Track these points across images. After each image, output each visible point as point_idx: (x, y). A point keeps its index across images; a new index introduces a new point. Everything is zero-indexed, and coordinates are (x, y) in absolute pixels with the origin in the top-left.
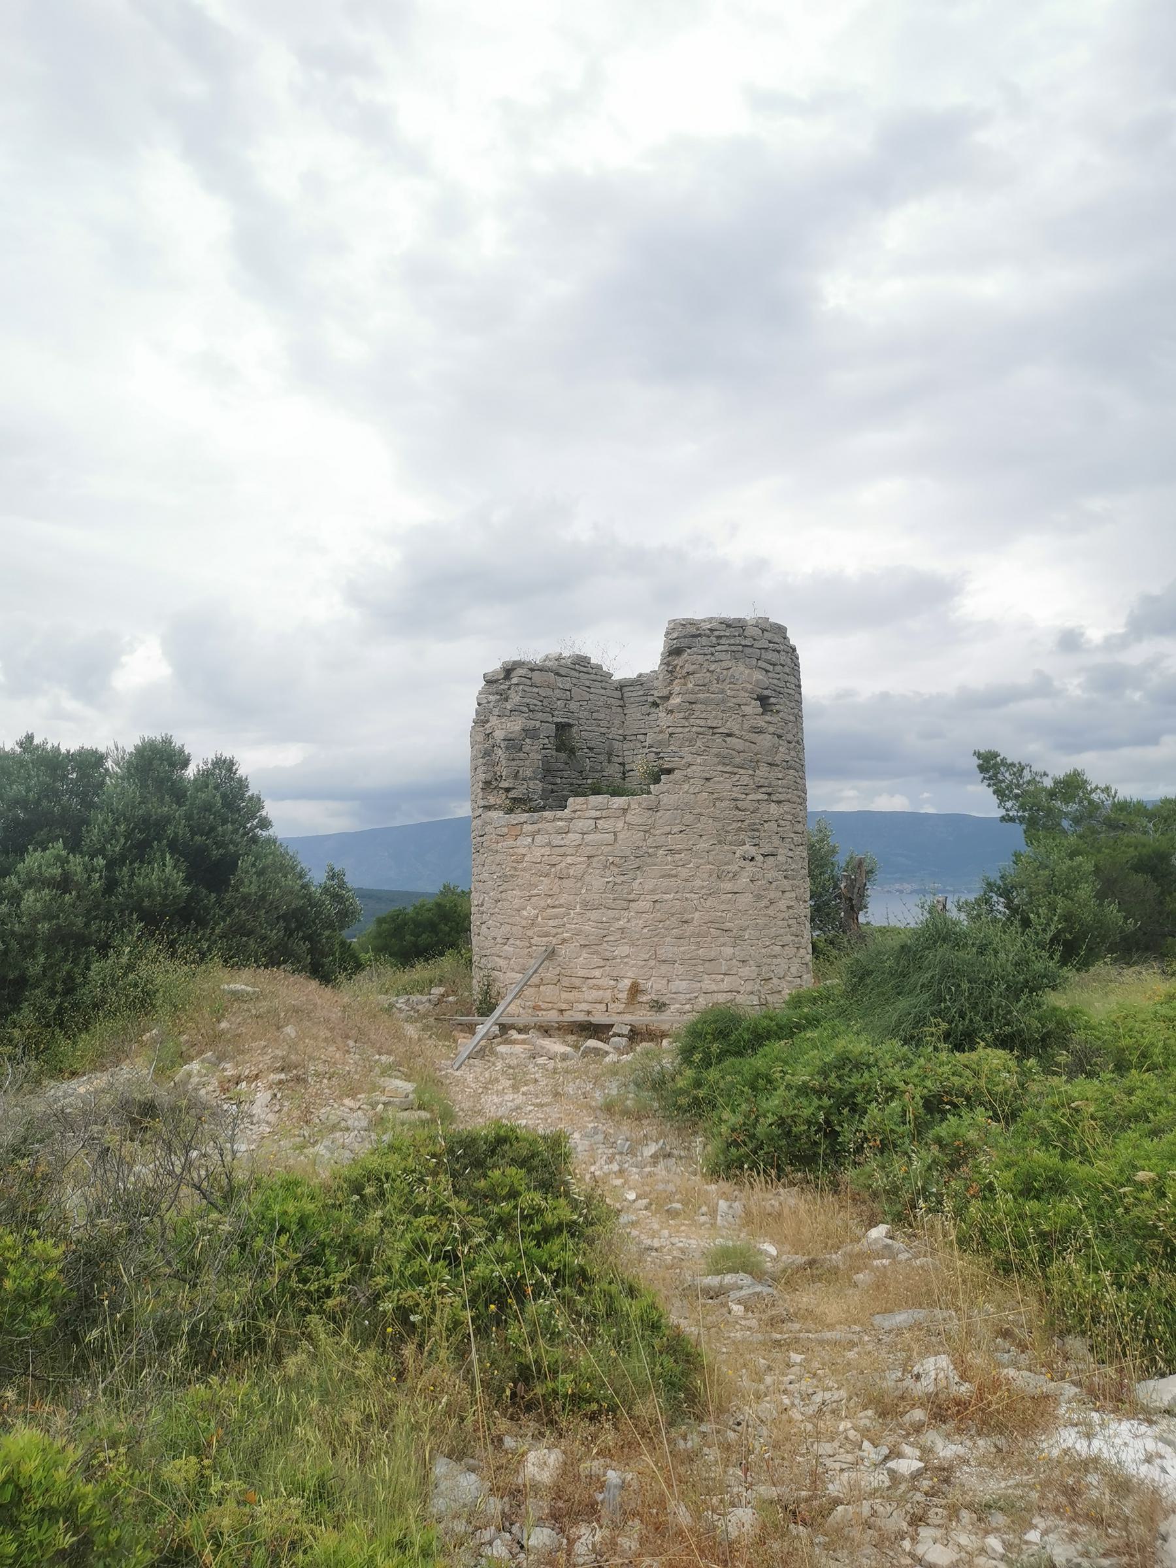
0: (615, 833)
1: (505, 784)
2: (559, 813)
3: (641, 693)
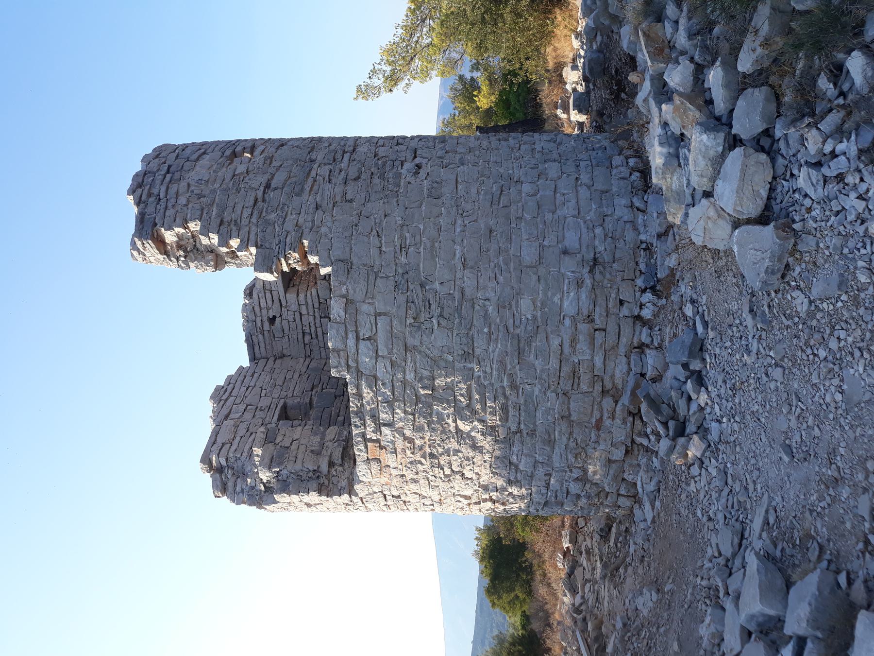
0: (377, 315)
1: (324, 468)
2: (351, 390)
3: (260, 336)
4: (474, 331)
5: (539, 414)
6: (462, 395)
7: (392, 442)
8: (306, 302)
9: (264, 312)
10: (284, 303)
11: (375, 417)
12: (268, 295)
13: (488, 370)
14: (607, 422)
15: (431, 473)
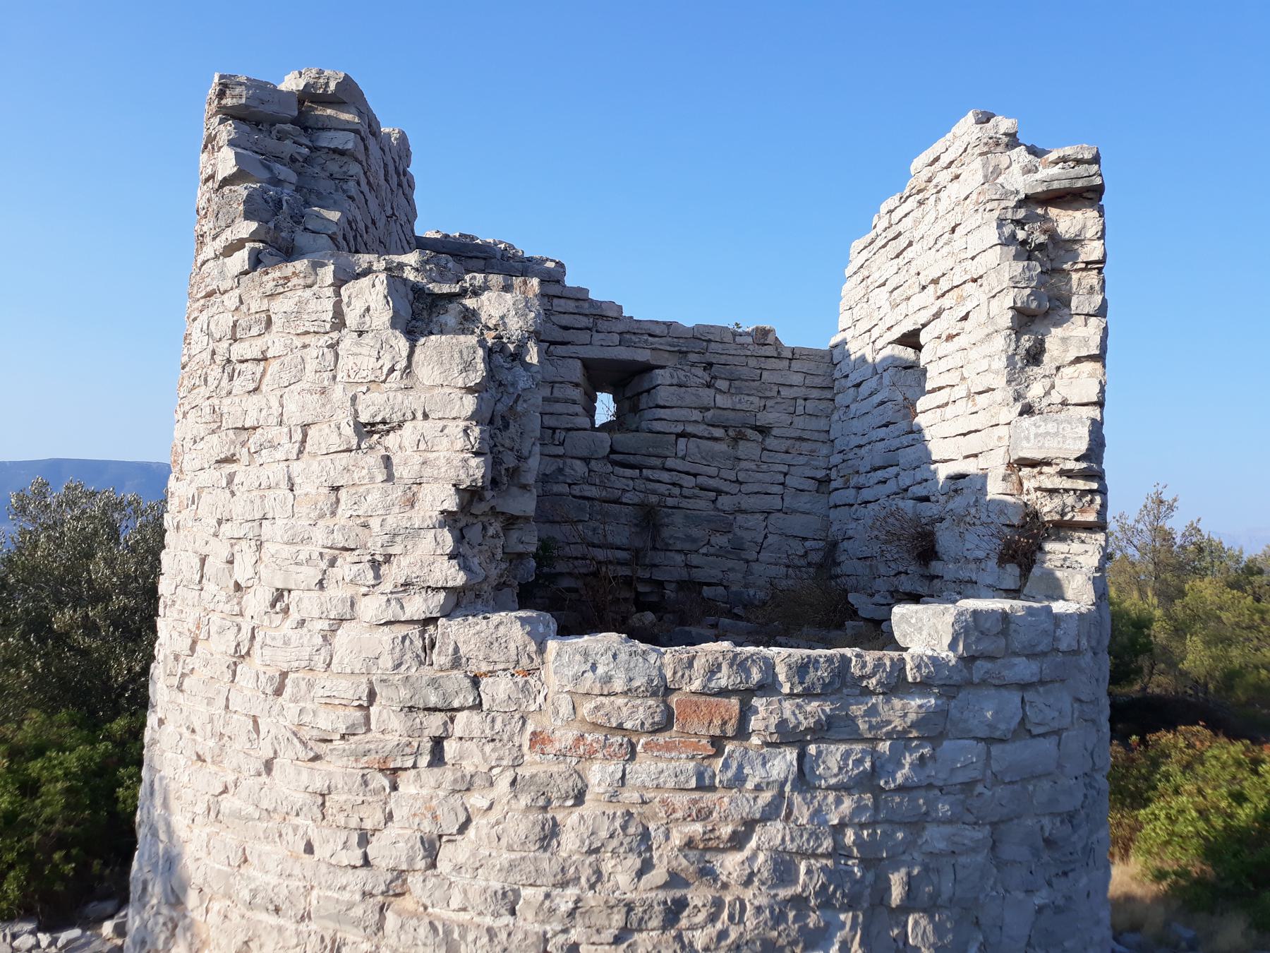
8: (557, 401)
10: (560, 350)
11: (825, 730)
12: (584, 322)
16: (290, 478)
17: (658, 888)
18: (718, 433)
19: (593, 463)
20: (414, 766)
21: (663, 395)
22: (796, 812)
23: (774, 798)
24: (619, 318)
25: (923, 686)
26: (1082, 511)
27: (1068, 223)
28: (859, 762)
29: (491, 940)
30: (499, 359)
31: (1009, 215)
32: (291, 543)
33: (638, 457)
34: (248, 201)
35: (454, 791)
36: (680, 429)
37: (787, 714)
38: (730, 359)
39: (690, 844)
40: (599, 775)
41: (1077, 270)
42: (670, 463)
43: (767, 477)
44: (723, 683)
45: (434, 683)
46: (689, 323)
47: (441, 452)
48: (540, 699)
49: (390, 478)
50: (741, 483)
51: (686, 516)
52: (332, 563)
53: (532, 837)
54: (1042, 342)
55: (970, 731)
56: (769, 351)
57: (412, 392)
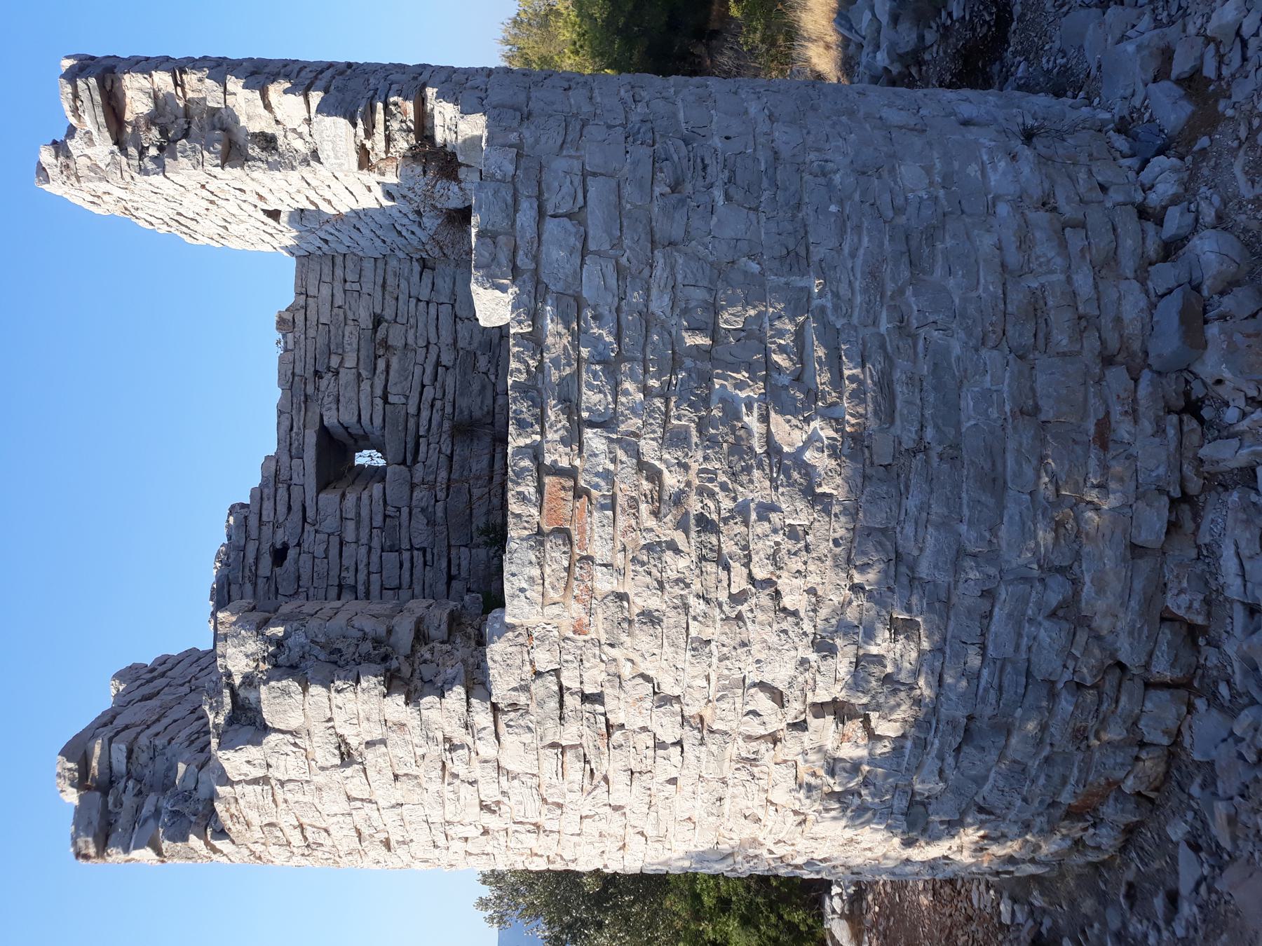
4: (807, 212)
5: (967, 403)
6: (782, 349)
7: (608, 476)
8: (358, 514)
9: (267, 530)
10: (311, 513)
11: (570, 405)
12: (282, 492)
13: (844, 290)
14: (1124, 429)
15: (696, 587)
16: (393, 807)
17: (688, 537)
18: (381, 364)
19: (415, 481)
20: (605, 714)
21: (349, 418)
22: (633, 429)
23: (621, 447)
24: (276, 459)
25: (535, 317)
26: (405, 113)
27: (138, 104)
28: (595, 374)
29: (727, 658)
30: (282, 659)
31: (136, 163)
32: (443, 804)
33: (408, 439)
34: (173, 839)
35: (621, 686)
36: (379, 401)
37: (557, 437)
38: (310, 355)
39: (656, 514)
40: (604, 583)
41: (184, 96)
42: (412, 410)
43: (422, 319)
44: (532, 490)
45: (541, 704)
46: (278, 393)
47: (361, 706)
48: (549, 628)
49: (383, 742)
50: (429, 343)
51: (462, 394)
52: (456, 776)
53: (651, 631)
54: (254, 135)
55: (575, 272)
56: (300, 317)
57: (312, 730)
